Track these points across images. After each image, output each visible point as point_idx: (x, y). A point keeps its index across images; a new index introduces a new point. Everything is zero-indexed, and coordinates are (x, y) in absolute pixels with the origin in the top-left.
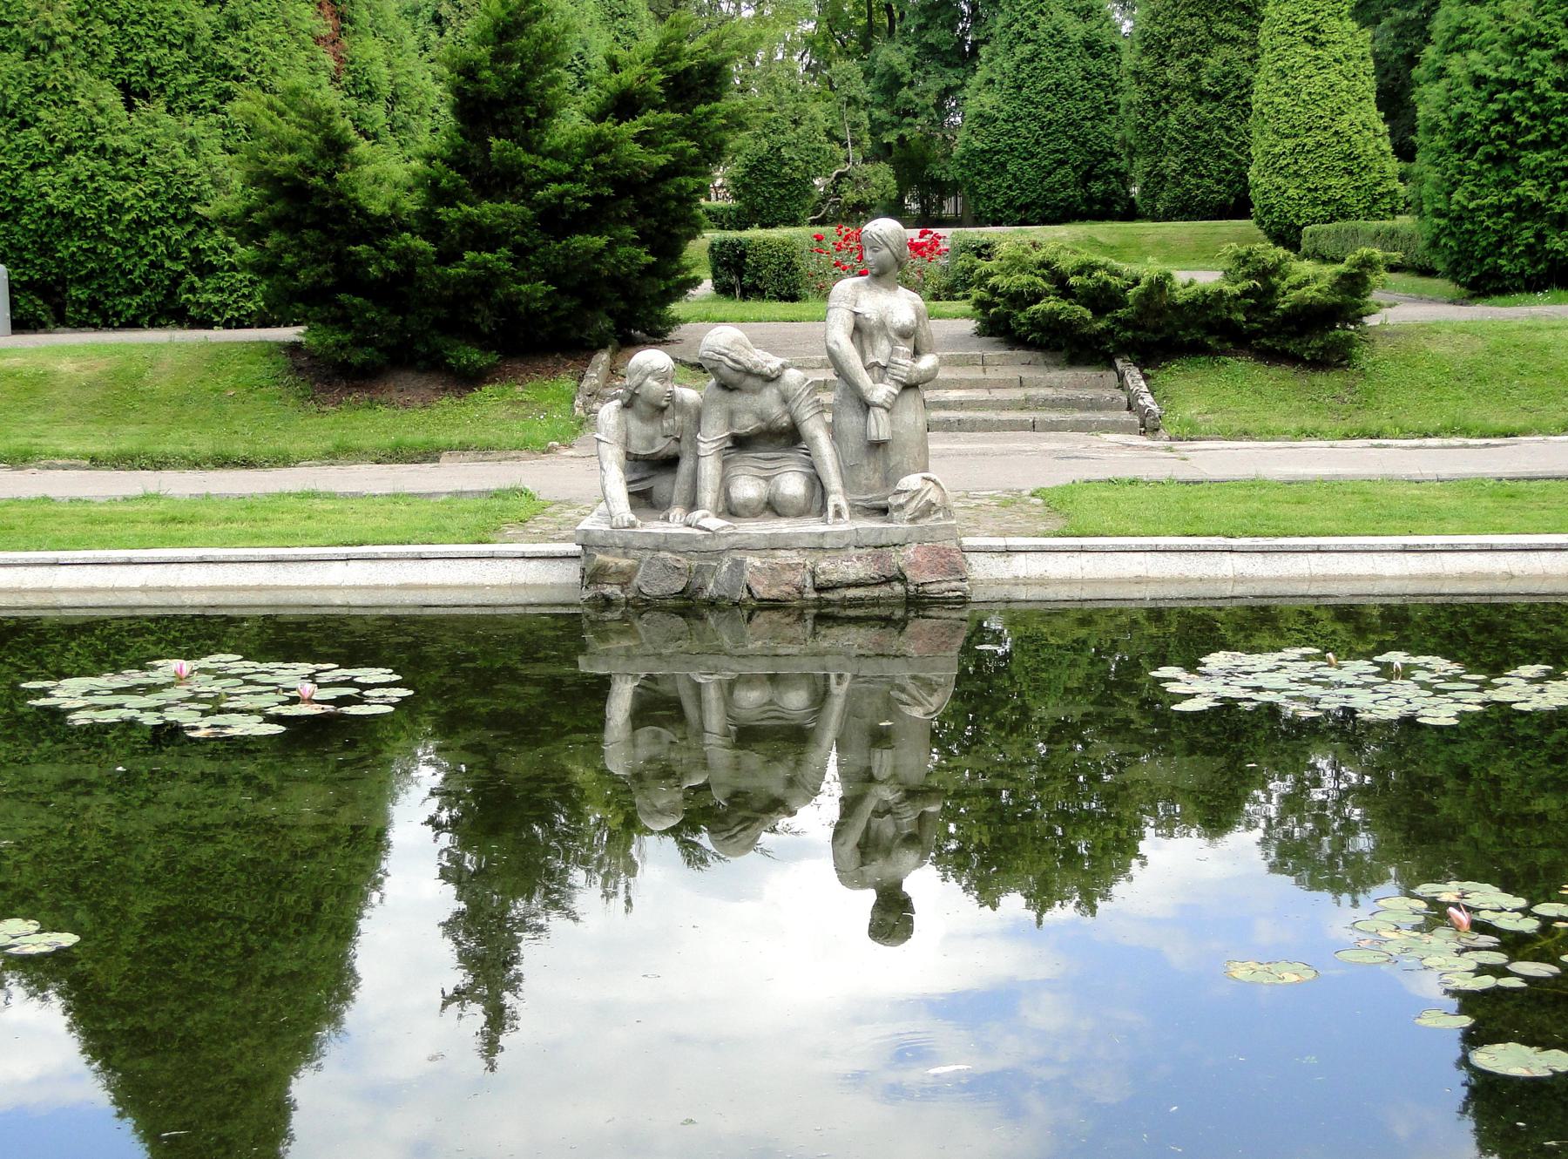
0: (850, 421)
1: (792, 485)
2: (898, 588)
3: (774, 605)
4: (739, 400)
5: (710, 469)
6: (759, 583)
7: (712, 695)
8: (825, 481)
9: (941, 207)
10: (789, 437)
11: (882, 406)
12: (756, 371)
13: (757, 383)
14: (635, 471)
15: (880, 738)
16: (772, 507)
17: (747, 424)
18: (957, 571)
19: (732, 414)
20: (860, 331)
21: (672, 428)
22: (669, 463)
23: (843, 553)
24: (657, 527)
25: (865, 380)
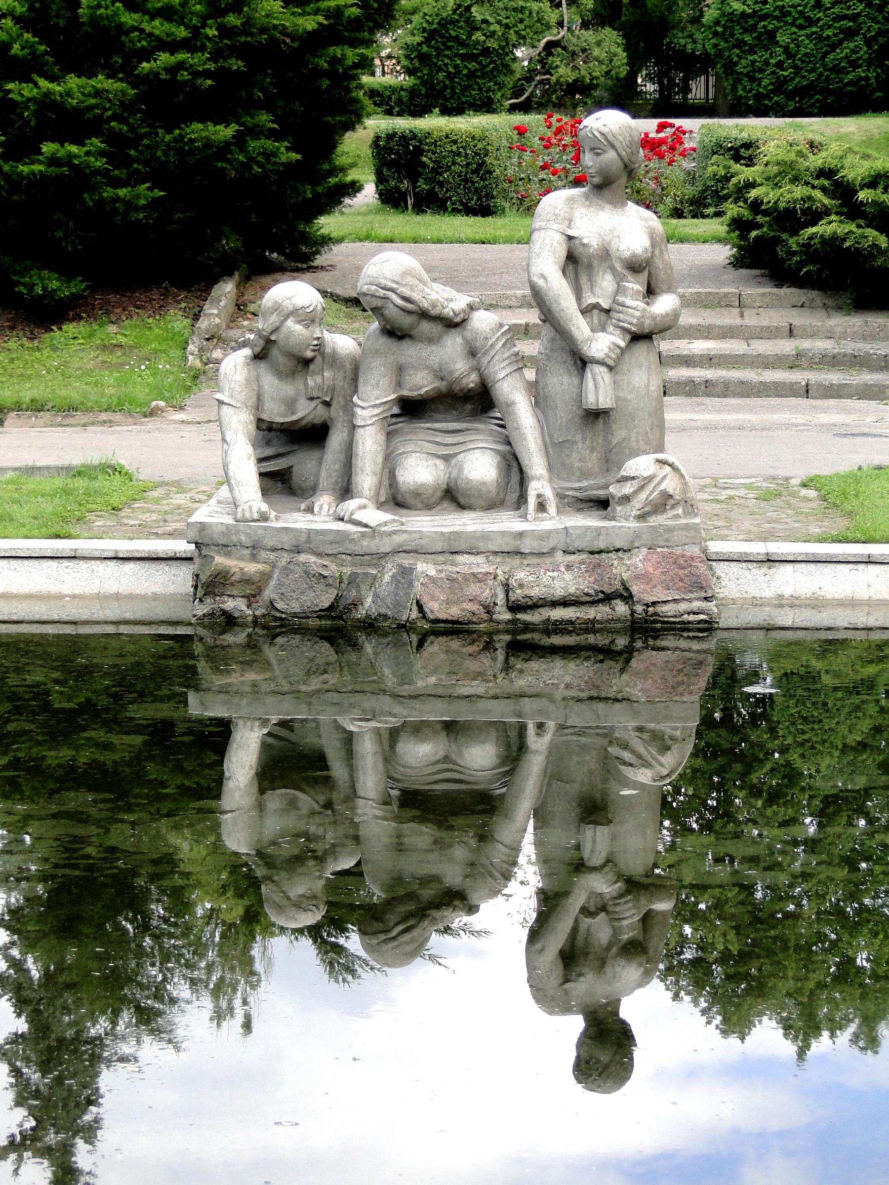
0: (560, 382)
1: (480, 466)
2: (621, 608)
3: (453, 629)
4: (410, 352)
5: (369, 444)
6: (433, 598)
7: (368, 749)
8: (525, 462)
9: (687, 89)
10: (476, 402)
12: (433, 312)
15: (594, 810)
16: (453, 496)
17: (421, 383)
18: (701, 587)
19: (400, 370)
20: (574, 261)
22: (312, 435)
23: (548, 560)
24: (297, 521)
25: (580, 327)
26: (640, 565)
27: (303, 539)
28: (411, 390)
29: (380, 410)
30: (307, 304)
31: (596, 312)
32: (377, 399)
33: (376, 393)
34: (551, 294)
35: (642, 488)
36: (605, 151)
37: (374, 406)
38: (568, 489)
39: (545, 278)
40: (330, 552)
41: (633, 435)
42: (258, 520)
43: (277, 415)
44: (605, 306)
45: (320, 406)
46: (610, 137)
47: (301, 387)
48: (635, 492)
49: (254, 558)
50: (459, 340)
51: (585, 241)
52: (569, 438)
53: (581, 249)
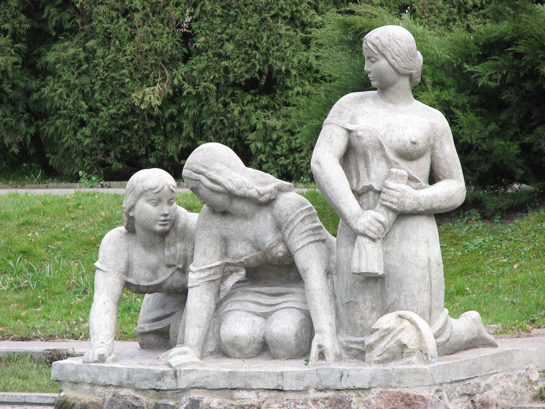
4: (232, 227)
11: (365, 235)
12: (239, 192)
13: (246, 208)
14: (163, 307)
16: (264, 348)
21: (174, 257)
25: (348, 204)
26: (373, 401)
27: (124, 377)
28: (234, 258)
29: (207, 273)
30: (154, 186)
31: (371, 193)
32: (204, 265)
33: (203, 260)
34: (323, 177)
35: (382, 338)
36: (378, 60)
37: (201, 271)
38: (352, 343)
39: (320, 164)
40: (143, 387)
41: (402, 297)
42: (97, 362)
43: (142, 280)
44: (377, 187)
45: (177, 273)
46: (380, 47)
47: (162, 256)
48: (378, 342)
49: (92, 392)
50: (269, 216)
51: (360, 133)
52: (352, 299)
53: (356, 141)
